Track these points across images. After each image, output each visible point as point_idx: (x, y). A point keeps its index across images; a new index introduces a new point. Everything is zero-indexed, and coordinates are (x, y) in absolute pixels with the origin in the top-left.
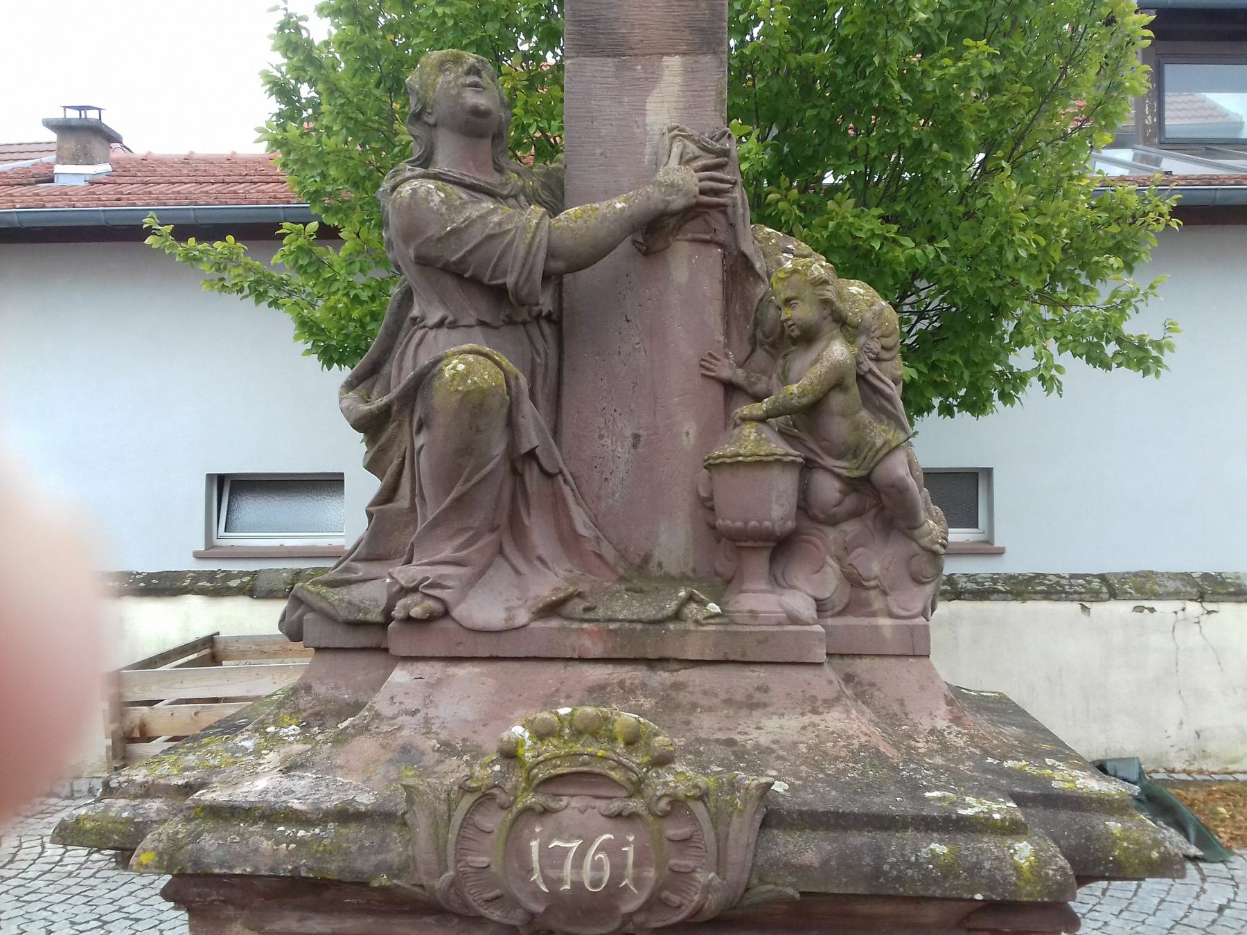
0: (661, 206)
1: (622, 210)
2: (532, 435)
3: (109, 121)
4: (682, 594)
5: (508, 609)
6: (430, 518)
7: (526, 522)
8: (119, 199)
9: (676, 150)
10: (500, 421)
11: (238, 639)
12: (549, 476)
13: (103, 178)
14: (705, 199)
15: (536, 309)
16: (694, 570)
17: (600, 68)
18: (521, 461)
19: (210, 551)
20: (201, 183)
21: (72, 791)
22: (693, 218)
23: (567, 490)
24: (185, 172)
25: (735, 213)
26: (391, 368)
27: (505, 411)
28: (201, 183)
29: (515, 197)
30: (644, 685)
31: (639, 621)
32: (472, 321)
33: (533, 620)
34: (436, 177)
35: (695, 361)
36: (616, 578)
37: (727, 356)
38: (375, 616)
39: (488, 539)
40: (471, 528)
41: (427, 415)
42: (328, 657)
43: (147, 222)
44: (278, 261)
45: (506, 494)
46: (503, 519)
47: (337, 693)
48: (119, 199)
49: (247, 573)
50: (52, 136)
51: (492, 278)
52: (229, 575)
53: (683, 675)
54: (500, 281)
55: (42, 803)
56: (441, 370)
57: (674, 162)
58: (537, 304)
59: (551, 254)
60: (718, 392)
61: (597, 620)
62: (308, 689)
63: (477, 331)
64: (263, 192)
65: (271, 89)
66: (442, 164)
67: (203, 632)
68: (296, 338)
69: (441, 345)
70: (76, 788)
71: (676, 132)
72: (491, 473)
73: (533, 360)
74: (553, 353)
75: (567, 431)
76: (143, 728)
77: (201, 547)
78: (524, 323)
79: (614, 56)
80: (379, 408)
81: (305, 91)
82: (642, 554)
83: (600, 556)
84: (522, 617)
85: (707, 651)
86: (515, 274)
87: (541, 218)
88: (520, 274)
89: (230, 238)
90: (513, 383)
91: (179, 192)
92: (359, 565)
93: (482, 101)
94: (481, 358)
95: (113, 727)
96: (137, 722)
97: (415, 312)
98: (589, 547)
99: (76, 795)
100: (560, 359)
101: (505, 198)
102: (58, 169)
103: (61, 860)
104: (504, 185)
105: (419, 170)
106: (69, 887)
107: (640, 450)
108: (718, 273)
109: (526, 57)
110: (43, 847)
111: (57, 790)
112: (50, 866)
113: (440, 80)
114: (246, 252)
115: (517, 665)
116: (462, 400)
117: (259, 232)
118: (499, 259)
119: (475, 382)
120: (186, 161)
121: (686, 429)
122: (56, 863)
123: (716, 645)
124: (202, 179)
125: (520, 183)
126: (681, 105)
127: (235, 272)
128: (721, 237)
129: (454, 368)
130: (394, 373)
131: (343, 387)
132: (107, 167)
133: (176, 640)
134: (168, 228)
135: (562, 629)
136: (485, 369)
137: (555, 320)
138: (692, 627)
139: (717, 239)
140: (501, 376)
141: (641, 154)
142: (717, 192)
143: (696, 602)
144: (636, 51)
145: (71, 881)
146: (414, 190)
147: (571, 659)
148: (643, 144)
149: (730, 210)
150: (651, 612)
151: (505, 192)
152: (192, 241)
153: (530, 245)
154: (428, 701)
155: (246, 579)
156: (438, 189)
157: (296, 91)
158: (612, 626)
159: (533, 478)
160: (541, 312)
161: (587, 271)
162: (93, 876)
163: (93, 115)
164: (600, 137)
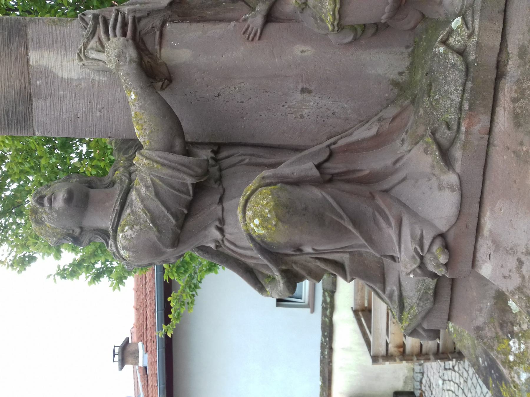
0: (134, 65)
1: (136, 94)
2: (307, 168)
3: (120, 343)
4: (442, 49)
5: (441, 188)
6: (363, 242)
7: (367, 172)
8: (154, 342)
9: (94, 55)
10: (298, 191)
11: (355, 300)
12: (331, 155)
13: (145, 346)
14: (129, 33)
15: (211, 162)
16: (407, 47)
17: (40, 110)
18: (326, 178)
19: (311, 306)
20: (146, 306)
21: (420, 373)
22: (144, 44)
23: (342, 142)
24: (141, 311)
25: (140, 11)
26: (250, 262)
27: (289, 187)
28: (146, 306)
29: (130, 174)
30: (518, 82)
31: (465, 84)
32: (219, 208)
33: (454, 171)
34: (115, 231)
35: (249, 44)
36: (412, 107)
37: (245, 20)
38: (431, 283)
39: (380, 201)
40: (373, 214)
41: (291, 247)
42: (454, 313)
43: (161, 335)
44: (181, 282)
45: (347, 187)
46: (364, 189)
47: (485, 310)
48: (154, 342)
49: (324, 293)
50: (126, 367)
51: (188, 193)
52: (324, 301)
53: (512, 48)
54: (190, 188)
55: (425, 386)
56: (259, 236)
57: (103, 56)
58: (208, 160)
59: (170, 149)
60: (272, 27)
61: (459, 119)
62: (478, 329)
63: (226, 204)
64: (150, 280)
65: (97, 281)
66: (107, 224)
67: (351, 314)
68: (216, 273)
69: (236, 231)
70: (418, 371)
71: (82, 56)
72: (335, 199)
73: (247, 164)
74: (241, 150)
75: (296, 141)
76: (399, 347)
77: (308, 310)
78: (220, 170)
79: (31, 100)
80: (283, 278)
81: (98, 265)
82: (391, 87)
83: (394, 119)
84: (452, 178)
85: (496, 27)
86: (185, 177)
87: (143, 155)
88: (185, 173)
89: (169, 299)
90: (268, 181)
91: (150, 316)
92: (388, 289)
93: (61, 196)
94: (249, 205)
95: (398, 360)
96: (396, 349)
97: (212, 245)
98: (386, 126)
99: (422, 371)
100: (246, 145)
101: (131, 181)
102: (141, 364)
103: (457, 384)
104: (121, 180)
105: (111, 242)
106: (473, 383)
107: (313, 88)
108: (185, 25)
109: (80, 160)
110: (449, 390)
111: (419, 379)
112: (460, 389)
113: (48, 224)
114: (176, 292)
115: (488, 183)
116: (283, 222)
117: (168, 288)
118: (174, 188)
119: (270, 211)
120: (137, 310)
121: (299, 53)
122: (459, 386)
123: (491, 20)
124: (145, 306)
125: (121, 169)
126: (64, 52)
127: (185, 297)
128: (158, 22)
129: (257, 227)
130: (254, 261)
131: (262, 294)
132: (140, 344)
133: (354, 326)
134: (164, 327)
135: (464, 147)
136: (258, 203)
137: (217, 148)
138: (475, 39)
139: (159, 26)
140: (264, 190)
141: (99, 82)
142: (124, 25)
143: (448, 39)
144: (27, 84)
145: (469, 382)
146: (124, 248)
147: (488, 141)
148: (92, 81)
149: (138, 15)
150: (457, 76)
151: (127, 181)
152: (170, 316)
153: (163, 165)
154: (511, 251)
155: (326, 294)
156: (123, 231)
157: (98, 269)
158: (466, 106)
159: (335, 167)
160: (212, 158)
161: (183, 124)
162: (467, 371)
163: (117, 350)
164: (88, 113)
